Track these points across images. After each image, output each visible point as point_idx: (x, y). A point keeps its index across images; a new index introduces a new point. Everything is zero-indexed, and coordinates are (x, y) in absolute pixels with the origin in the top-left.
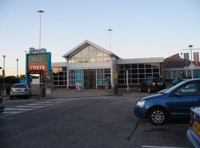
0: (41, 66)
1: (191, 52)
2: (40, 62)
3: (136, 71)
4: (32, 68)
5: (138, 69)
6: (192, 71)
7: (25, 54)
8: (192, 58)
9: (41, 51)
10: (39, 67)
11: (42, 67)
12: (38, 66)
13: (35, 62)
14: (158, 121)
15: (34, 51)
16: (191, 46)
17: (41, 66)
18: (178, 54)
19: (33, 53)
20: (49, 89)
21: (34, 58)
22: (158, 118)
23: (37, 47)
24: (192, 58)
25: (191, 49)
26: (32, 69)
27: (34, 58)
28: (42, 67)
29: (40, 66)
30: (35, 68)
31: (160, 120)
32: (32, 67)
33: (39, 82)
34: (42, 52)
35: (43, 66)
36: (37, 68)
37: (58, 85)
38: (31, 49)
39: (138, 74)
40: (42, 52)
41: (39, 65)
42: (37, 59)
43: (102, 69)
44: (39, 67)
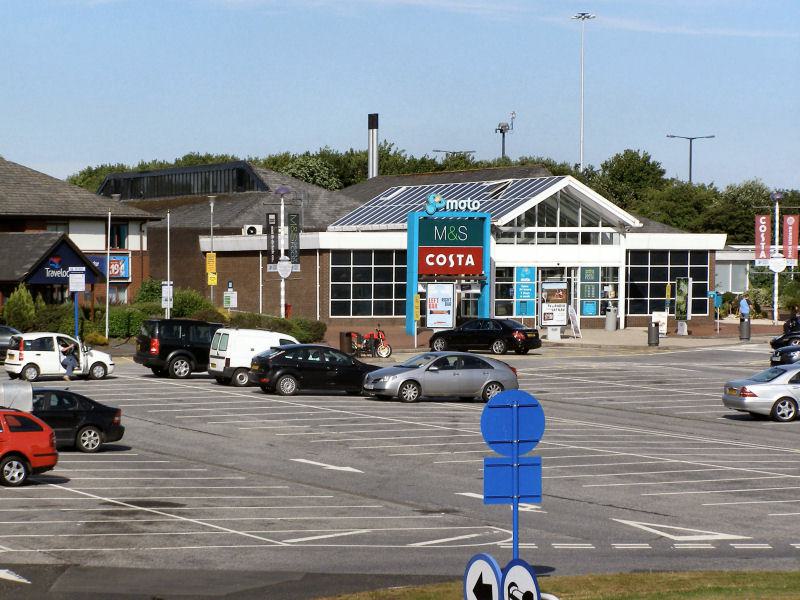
2: (461, 243)
3: (364, 275)
4: (431, 260)
5: (649, 266)
6: (211, 190)
10: (456, 259)
11: (464, 260)
14: (90, 433)
22: (90, 439)
26: (432, 264)
28: (464, 260)
29: (460, 257)
30: (441, 260)
31: (85, 435)
33: (133, 249)
35: (470, 256)
36: (448, 262)
37: (393, 316)
39: (352, 283)
41: (456, 252)
42: (448, 231)
43: (596, 269)
44: (456, 259)
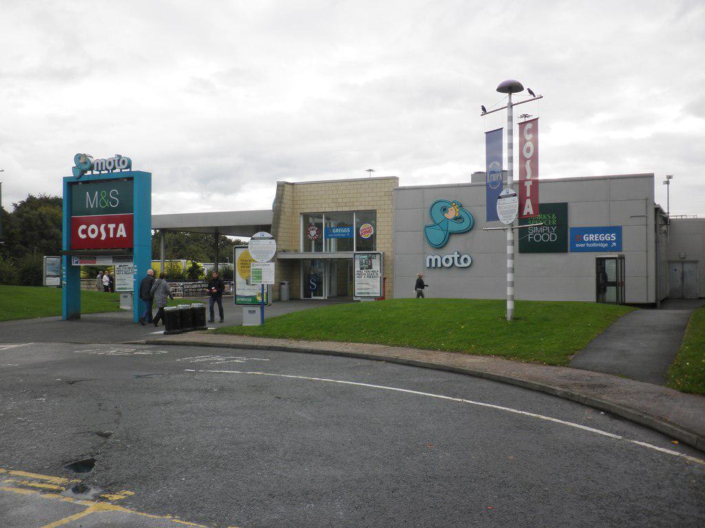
0: (114, 225)
1: (510, 119)
4: (84, 232)
7: (619, 225)
8: (511, 160)
9: (114, 168)
10: (107, 230)
11: (115, 230)
12: (103, 226)
13: (98, 211)
15: (87, 166)
16: (511, 88)
17: (114, 225)
18: (651, 176)
19: (89, 173)
20: (254, 312)
21: (92, 197)
23: (99, 154)
24: (511, 160)
25: (511, 106)
26: (83, 237)
27: (92, 197)
28: (115, 230)
29: (112, 226)
30: (93, 231)
32: (84, 227)
34: (117, 170)
35: (121, 226)
38: (78, 157)
40: (117, 170)
41: (108, 221)
42: (99, 197)
44: (107, 230)
